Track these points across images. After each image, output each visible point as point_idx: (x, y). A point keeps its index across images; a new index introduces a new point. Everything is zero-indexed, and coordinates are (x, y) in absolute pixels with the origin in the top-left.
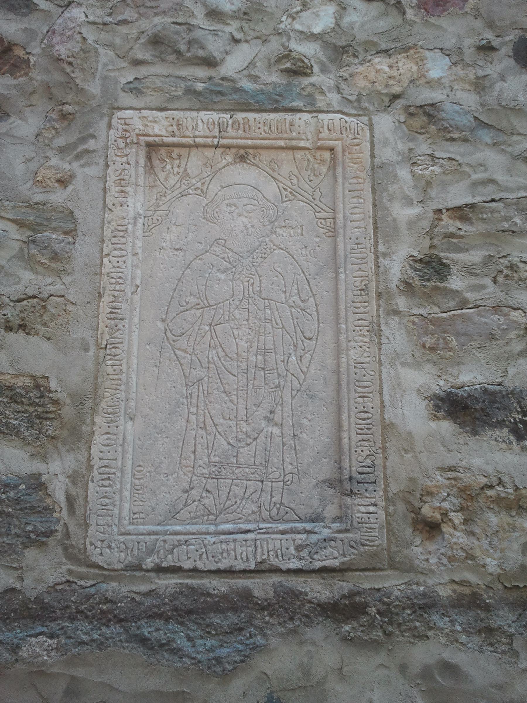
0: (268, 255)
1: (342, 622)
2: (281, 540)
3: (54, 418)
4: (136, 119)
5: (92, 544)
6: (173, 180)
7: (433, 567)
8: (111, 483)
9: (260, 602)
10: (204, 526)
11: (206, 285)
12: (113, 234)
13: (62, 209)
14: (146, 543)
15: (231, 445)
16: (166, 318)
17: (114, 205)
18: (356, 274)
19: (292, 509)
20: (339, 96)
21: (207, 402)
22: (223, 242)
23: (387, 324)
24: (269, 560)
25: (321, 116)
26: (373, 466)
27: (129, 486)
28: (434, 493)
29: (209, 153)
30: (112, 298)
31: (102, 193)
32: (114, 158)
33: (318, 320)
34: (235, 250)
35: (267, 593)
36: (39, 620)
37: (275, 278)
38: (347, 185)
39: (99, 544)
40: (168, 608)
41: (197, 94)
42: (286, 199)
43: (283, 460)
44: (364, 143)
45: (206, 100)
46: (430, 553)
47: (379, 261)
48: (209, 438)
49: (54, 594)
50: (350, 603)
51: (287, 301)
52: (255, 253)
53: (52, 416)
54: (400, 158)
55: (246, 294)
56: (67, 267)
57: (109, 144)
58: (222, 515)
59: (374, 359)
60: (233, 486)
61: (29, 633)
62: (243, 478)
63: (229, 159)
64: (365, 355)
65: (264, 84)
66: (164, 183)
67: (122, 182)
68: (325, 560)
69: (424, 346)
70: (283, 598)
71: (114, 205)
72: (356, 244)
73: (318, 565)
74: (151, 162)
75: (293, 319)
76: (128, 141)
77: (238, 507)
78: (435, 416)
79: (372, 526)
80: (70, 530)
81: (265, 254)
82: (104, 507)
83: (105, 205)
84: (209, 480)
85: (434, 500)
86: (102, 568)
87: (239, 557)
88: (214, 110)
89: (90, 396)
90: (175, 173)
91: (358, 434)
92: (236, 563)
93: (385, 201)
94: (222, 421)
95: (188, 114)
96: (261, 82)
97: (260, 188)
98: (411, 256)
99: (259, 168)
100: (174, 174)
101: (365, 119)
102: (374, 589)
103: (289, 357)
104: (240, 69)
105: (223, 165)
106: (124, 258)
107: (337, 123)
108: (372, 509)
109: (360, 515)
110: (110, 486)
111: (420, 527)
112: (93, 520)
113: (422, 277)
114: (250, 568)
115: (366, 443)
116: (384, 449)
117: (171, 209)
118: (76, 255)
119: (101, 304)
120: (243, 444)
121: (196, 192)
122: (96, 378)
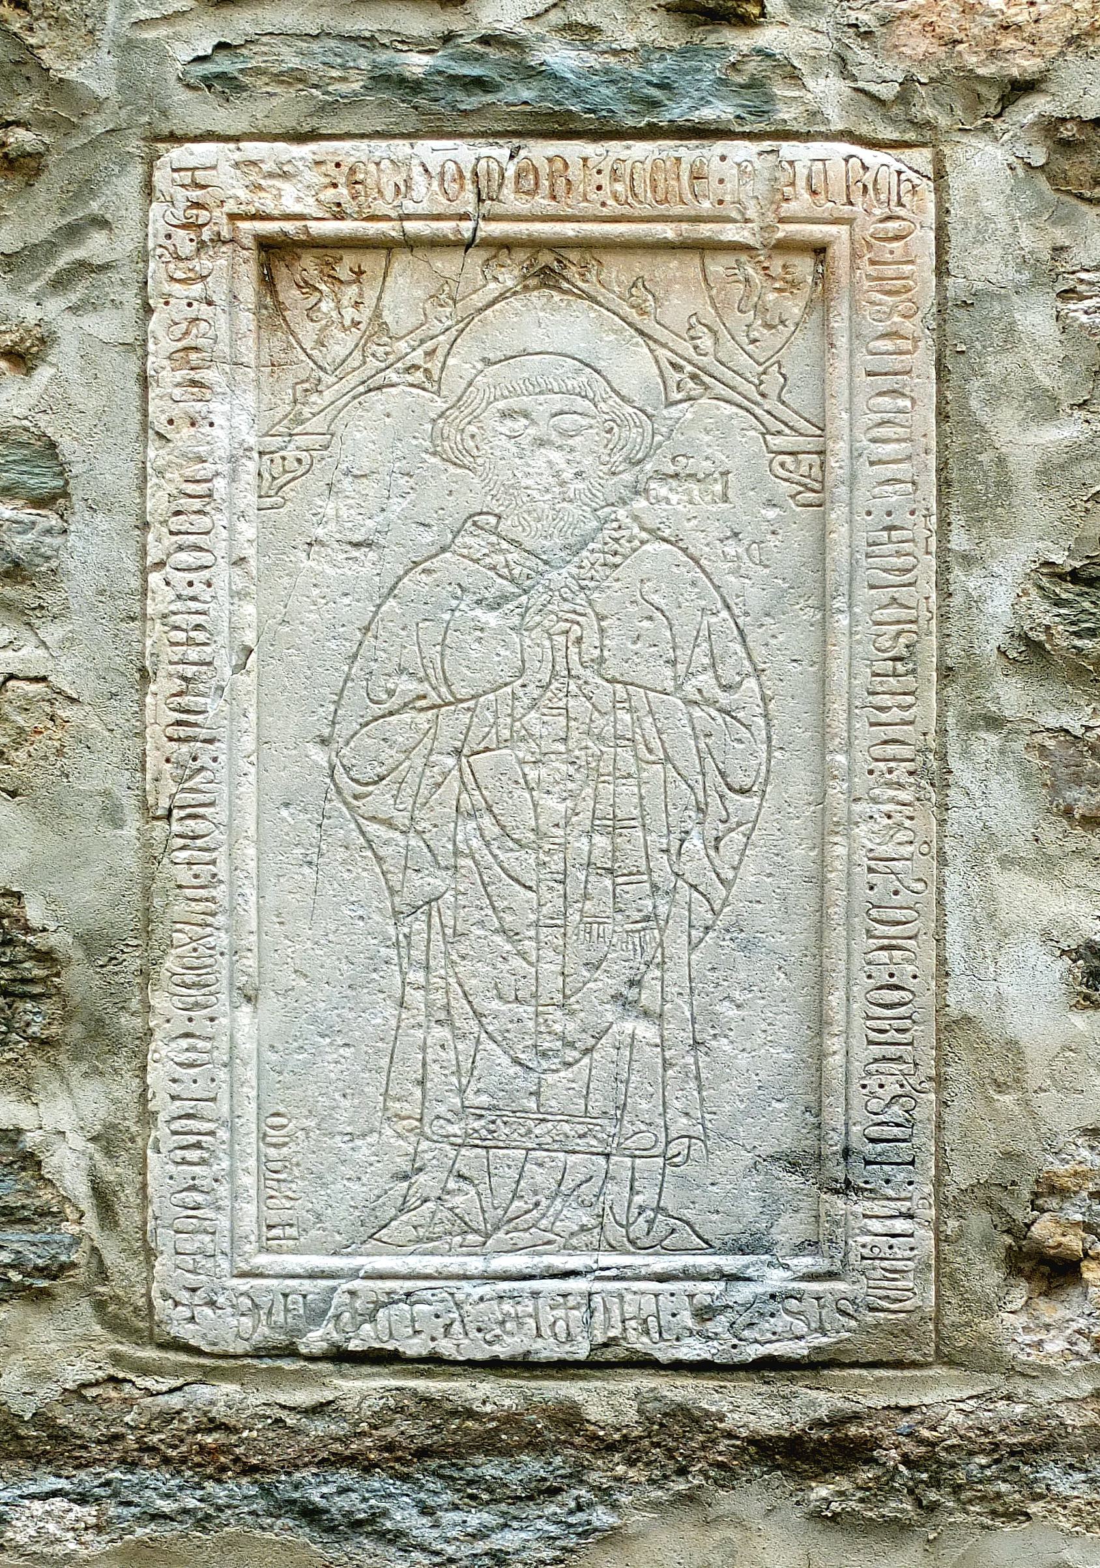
0: (625, 557)
1: (810, 1478)
2: (656, 1296)
3: (42, 995)
4: (225, 167)
5: (166, 1296)
6: (341, 344)
7: (1052, 1362)
8: (206, 1155)
9: (601, 1433)
10: (454, 1259)
11: (443, 644)
12: (174, 507)
13: (25, 437)
14: (305, 1296)
15: (521, 1064)
16: (331, 736)
17: (171, 422)
18: (879, 615)
19: (688, 1223)
20: (843, 87)
21: (455, 957)
22: (493, 520)
23: (966, 753)
24: (625, 1339)
25: (788, 149)
26: (911, 1123)
27: (252, 1163)
28: (1068, 1190)
29: (446, 264)
30: (177, 685)
31: (136, 389)
32: (167, 287)
33: (769, 738)
34: (528, 544)
35: (620, 1413)
36: (49, 1462)
37: (646, 624)
38: (862, 357)
39: (184, 1296)
40: (368, 1442)
41: (411, 86)
42: (679, 396)
43: (664, 1103)
44: (918, 233)
45: (435, 107)
46: (1048, 1327)
47: (951, 577)
48: (460, 1047)
49: (79, 1407)
50: (833, 1439)
51: (679, 687)
52: (585, 553)
53: (37, 990)
54: (1026, 275)
55: (561, 667)
56: (49, 597)
57: (151, 245)
58: (501, 1234)
59: (925, 849)
60: (528, 1166)
61: (26, 1492)
62: (556, 1147)
63: (509, 278)
64: (901, 836)
65: (615, 53)
66: (315, 353)
67: (193, 356)
68: (770, 1342)
69: (1068, 812)
70: (661, 1425)
71: (171, 422)
72: (885, 529)
73: (753, 1352)
74: (274, 293)
75: (696, 738)
76: (206, 234)
77: (544, 1215)
78: (1086, 997)
79: (899, 1265)
80: (108, 1263)
81: (616, 553)
82: (191, 1213)
83: (145, 425)
84: (463, 1151)
85: (1066, 1205)
86: (198, 1352)
87: (546, 1331)
88: (461, 135)
89: (135, 942)
90: (347, 323)
91: (870, 1043)
92: (539, 1344)
93: (974, 404)
94: (496, 1005)
95: (381, 147)
96: (604, 47)
97: (600, 365)
98: (1047, 564)
99: (598, 303)
100: (345, 329)
101: (921, 158)
102: (897, 1407)
103: (682, 841)
104: (540, 8)
105: (491, 297)
106: (206, 574)
107: (837, 169)
108: (900, 1225)
109: (867, 1239)
110: (203, 1162)
111: (1027, 1266)
112: (164, 1240)
113: (1072, 623)
114: (576, 1357)
115: (895, 1067)
116: (940, 1081)
117: (340, 430)
118: (71, 565)
119: (149, 699)
120: (555, 1063)
121: (410, 379)
122: (147, 893)
